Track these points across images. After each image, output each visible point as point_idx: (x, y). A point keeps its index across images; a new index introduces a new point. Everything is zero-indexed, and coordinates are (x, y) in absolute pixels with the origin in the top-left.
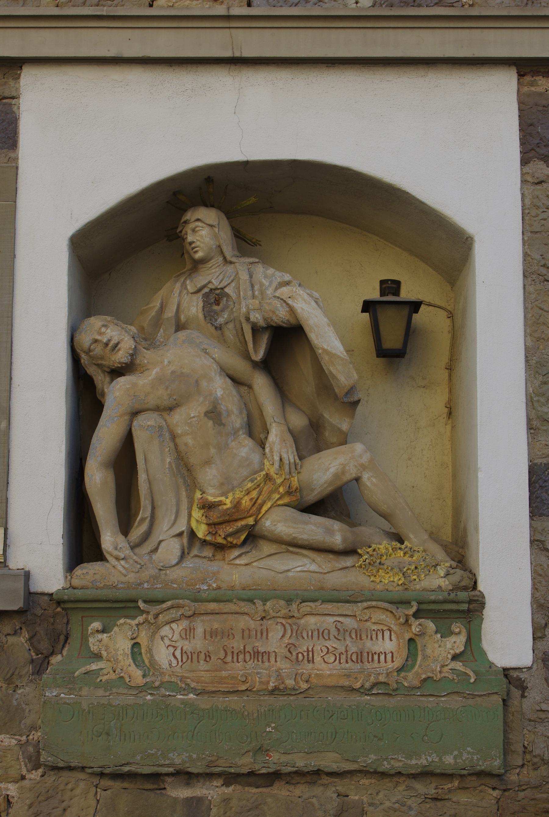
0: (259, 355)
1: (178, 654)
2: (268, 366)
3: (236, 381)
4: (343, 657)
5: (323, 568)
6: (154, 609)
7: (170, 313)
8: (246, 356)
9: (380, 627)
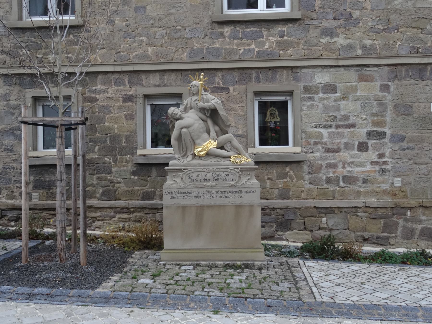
0: (208, 115)
6: (185, 171)
7: (189, 106)
8: (205, 115)
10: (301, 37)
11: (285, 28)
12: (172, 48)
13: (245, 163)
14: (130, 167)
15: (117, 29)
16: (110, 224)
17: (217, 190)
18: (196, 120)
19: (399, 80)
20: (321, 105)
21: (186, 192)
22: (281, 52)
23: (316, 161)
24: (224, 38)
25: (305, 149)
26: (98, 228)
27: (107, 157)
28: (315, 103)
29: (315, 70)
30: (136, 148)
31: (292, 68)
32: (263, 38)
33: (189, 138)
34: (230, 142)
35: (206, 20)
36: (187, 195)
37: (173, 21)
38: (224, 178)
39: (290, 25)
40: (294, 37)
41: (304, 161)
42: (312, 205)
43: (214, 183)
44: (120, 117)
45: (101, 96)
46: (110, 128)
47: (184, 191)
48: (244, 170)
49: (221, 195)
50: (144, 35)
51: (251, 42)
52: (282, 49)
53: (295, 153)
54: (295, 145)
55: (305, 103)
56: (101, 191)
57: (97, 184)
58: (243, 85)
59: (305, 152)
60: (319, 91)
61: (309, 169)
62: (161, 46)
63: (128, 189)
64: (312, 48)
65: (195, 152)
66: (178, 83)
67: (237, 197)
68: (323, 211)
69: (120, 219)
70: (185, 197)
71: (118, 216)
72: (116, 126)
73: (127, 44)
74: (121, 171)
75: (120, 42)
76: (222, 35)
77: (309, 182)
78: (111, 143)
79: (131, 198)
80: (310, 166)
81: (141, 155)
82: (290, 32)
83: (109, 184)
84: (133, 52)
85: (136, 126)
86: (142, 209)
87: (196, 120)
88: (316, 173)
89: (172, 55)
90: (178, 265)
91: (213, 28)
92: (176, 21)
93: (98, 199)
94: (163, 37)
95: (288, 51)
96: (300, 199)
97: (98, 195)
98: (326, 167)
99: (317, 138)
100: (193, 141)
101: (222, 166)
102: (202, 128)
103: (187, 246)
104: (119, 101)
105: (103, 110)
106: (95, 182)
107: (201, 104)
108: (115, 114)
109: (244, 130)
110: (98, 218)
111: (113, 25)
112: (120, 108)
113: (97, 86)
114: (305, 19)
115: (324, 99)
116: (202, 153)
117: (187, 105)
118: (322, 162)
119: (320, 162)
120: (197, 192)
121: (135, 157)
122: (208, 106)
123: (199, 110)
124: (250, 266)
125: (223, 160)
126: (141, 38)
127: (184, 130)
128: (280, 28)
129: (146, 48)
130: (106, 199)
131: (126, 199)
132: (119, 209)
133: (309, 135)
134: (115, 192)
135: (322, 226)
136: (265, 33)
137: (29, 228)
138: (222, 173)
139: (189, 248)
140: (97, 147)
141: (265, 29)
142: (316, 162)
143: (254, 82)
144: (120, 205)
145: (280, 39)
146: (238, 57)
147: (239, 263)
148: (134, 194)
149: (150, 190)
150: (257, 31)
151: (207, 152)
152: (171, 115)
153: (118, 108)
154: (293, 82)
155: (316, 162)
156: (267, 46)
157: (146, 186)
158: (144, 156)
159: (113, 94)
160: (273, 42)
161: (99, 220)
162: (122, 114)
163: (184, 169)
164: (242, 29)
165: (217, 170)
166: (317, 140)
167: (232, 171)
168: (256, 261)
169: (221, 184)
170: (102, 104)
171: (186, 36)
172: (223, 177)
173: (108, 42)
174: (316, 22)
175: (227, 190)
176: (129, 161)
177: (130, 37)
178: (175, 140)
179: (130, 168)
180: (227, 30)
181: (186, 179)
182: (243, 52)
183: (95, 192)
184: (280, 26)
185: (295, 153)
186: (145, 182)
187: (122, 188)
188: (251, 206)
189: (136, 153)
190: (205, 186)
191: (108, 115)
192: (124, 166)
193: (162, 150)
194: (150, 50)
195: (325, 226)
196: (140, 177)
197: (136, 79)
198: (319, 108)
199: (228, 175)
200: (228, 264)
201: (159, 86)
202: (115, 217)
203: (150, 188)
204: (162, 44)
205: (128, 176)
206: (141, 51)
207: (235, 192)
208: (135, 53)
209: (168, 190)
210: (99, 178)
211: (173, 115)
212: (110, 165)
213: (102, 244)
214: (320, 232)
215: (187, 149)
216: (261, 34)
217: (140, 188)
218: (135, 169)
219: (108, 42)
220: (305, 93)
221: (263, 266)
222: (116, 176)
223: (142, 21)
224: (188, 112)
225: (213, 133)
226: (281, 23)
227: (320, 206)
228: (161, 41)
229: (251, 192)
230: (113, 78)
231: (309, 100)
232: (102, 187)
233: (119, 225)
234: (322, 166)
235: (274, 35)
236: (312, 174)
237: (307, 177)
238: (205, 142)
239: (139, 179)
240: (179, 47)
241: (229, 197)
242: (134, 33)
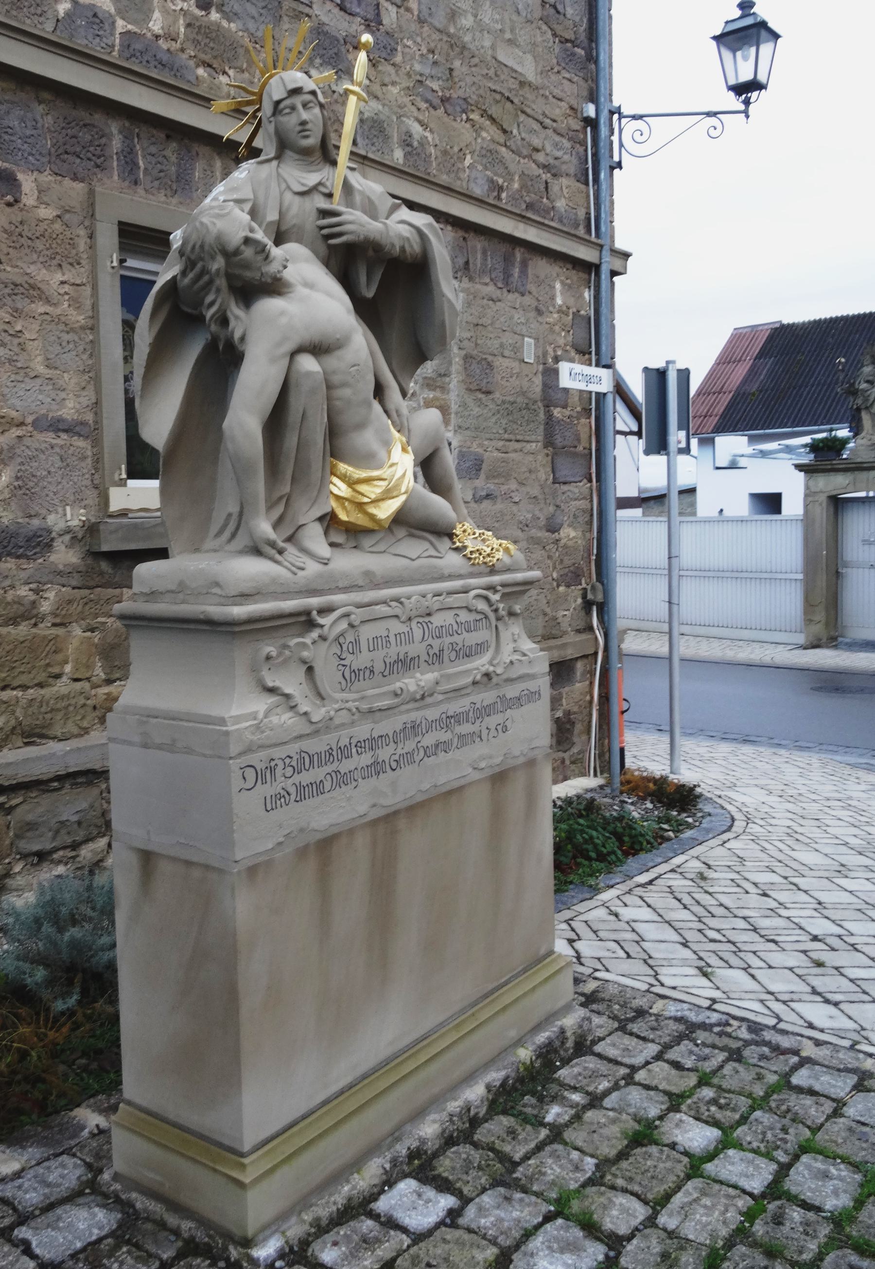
19: (471, 279)
36: (334, 767)
58: (75, 178)
109: (85, 401)
139: (349, 1079)
143: (116, 178)
207: (487, 711)
211: (248, 253)
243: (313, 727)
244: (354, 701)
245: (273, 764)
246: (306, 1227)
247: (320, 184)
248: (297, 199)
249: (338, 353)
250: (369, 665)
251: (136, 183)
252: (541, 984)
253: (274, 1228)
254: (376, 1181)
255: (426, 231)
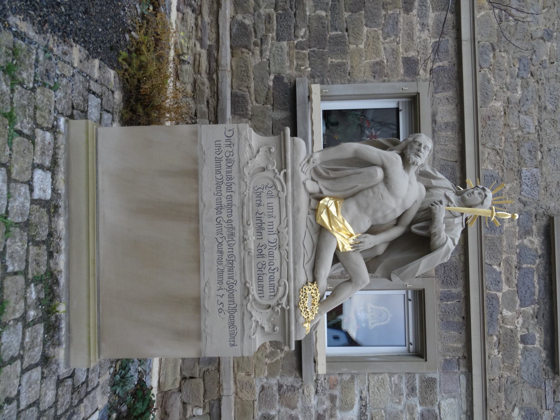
0: (413, 228)
1: (260, 190)
2: (408, 235)
3: (399, 219)
4: (260, 272)
5: (314, 328)
6: (281, 177)
7: (434, 182)
8: (413, 222)
9: (276, 290)
10: (522, 373)
11: (538, 346)
12: (503, 144)
13: (301, 320)
14: (289, 72)
15: (536, 45)
16: (190, 38)
17: (236, 253)
18: (404, 201)
20: (400, 407)
21: (231, 179)
22: (495, 338)
23: (302, 399)
24: (521, 237)
25: (322, 379)
26: (183, 18)
27: (307, 32)
28: (404, 398)
29: (464, 398)
30: (322, 83)
31: (468, 358)
32: (521, 306)
33: (361, 186)
34: (350, 281)
35: (552, 205)
36: (225, 181)
37: (551, 146)
38: (266, 271)
39: (544, 355)
40: (522, 361)
41: (302, 377)
42: (225, 392)
43: (252, 246)
44: (377, 53)
45: (415, 18)
46: (357, 36)
47: (235, 173)
48: (284, 317)
49: (225, 262)
50: (526, 93)
51: (514, 285)
52: (502, 340)
53: (315, 362)
54: (331, 360)
55: (404, 380)
56: (247, 22)
57: (259, 16)
59: (317, 379)
60: (426, 405)
61: (287, 386)
62: (505, 125)
63: (251, 69)
64: (503, 393)
65: (327, 199)
66: (439, 156)
67: (221, 300)
68: (214, 410)
69: (198, 57)
70: (219, 176)
71: (204, 53)
72: (362, 46)
73: (509, 63)
74: (281, 57)
75: (511, 52)
76: (528, 232)
77: (265, 385)
78: (331, 38)
79: (235, 75)
80: (293, 388)
81: (310, 91)
82: (532, 354)
83: (259, 36)
84: (494, 74)
85: (361, 82)
86: (216, 94)
87: (404, 201)
88: (280, 398)
89: (490, 144)
90: (55, 162)
91: (538, 217)
92: (552, 151)
93: (233, 18)
94: (521, 128)
95: (496, 351)
96: (236, 369)
97: (239, 17)
98: (291, 416)
99: (342, 401)
100: (353, 195)
101: (295, 263)
102: (385, 216)
103: (104, 182)
104: (406, 51)
105: (391, 22)
106: (262, 11)
107: (441, 213)
108: (385, 45)
110: (199, 17)
111: (542, 38)
112: (394, 52)
113: (433, 12)
114: (556, 381)
115: (412, 414)
116: (324, 217)
117: (435, 178)
118: (299, 410)
119: (299, 405)
120: (230, 205)
121: (307, 81)
122: (440, 232)
123: (426, 206)
124: (53, 336)
125: (308, 267)
126: (519, 89)
127: (380, 173)
128: (539, 337)
129: (502, 98)
130: (234, 31)
131: (234, 68)
132: (216, 55)
133: (347, 387)
134: (246, 47)
135: (189, 408)
136: (530, 310)
137: (363, 320)
138: (277, 264)
139: (100, 187)
140: (324, 14)
141: (536, 310)
142: (300, 399)
143: (441, 290)
144: (223, 55)
145: (519, 336)
146: (487, 261)
147: (62, 308)
148: (242, 80)
149: (249, 108)
150: (534, 295)
151: (327, 230)
152: (414, 142)
153: (393, 50)
154: (441, 359)
155: (300, 399)
156: (506, 313)
157: (257, 101)
158: (309, 97)
159: (418, 40)
160: (513, 324)
161: (196, 19)
162: (383, 56)
163: (285, 174)
164: (537, 268)
165: (284, 253)
166: (338, 400)
167: (281, 289)
168: (68, 349)
169: (250, 263)
170: (402, 21)
171: (524, 169)
172: (268, 267)
173: (512, 30)
174: (550, 400)
175: (237, 277)
176: (300, 70)
177: (522, 68)
178: (356, 151)
179: (288, 72)
180: (535, 242)
181: (262, 179)
182: (495, 270)
183: (245, 11)
184: (543, 336)
185: (315, 362)
186: (262, 99)
187: (251, 59)
188: (199, 335)
189: (315, 83)
190: (245, 225)
191: (380, 32)
192: (291, 62)
193: (319, 127)
194: (499, 105)
195: (189, 414)
196: (272, 91)
197: (445, 81)
198: (396, 406)
199: (271, 279)
200: (57, 283)
201: (434, 121)
202: (202, 47)
203: (253, 108)
204: (508, 126)
205: (273, 69)
206: (496, 89)
207: (231, 297)
208: (492, 79)
209: (235, 136)
210: (270, 18)
211: (416, 146)
212: (293, 37)
213: (139, 10)
214: (179, 404)
215: (334, 179)
216: (527, 303)
217: (252, 90)
218: (286, 81)
219: (512, 30)
220: (422, 381)
221: (54, 367)
222: (274, 49)
223: (552, 89)
224: (418, 180)
225: (371, 241)
226: (548, 339)
227: (222, 407)
228: (514, 125)
229: (233, 336)
230: (448, 40)
231: (410, 387)
232: (254, 24)
233: (187, 54)
234: (294, 408)
235: (526, 325)
236: (279, 390)
237: (273, 382)
238: (351, 224)
239: (269, 89)
240: (505, 156)
241: (220, 282)
242: (529, 75)
243: (242, 168)
244: (249, 193)
245: (232, 145)
246: (59, 144)
247: (452, 203)
248: (443, 194)
249: (386, 189)
250: (262, 203)
251: (441, 300)
252: (89, 333)
253: (66, 132)
254: (57, 184)
255: (446, 246)
